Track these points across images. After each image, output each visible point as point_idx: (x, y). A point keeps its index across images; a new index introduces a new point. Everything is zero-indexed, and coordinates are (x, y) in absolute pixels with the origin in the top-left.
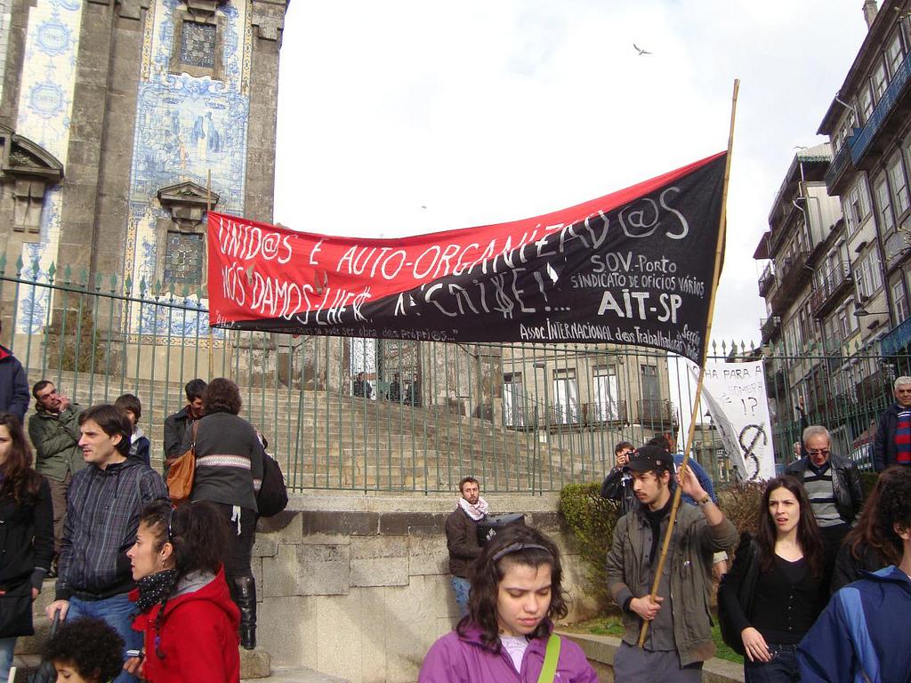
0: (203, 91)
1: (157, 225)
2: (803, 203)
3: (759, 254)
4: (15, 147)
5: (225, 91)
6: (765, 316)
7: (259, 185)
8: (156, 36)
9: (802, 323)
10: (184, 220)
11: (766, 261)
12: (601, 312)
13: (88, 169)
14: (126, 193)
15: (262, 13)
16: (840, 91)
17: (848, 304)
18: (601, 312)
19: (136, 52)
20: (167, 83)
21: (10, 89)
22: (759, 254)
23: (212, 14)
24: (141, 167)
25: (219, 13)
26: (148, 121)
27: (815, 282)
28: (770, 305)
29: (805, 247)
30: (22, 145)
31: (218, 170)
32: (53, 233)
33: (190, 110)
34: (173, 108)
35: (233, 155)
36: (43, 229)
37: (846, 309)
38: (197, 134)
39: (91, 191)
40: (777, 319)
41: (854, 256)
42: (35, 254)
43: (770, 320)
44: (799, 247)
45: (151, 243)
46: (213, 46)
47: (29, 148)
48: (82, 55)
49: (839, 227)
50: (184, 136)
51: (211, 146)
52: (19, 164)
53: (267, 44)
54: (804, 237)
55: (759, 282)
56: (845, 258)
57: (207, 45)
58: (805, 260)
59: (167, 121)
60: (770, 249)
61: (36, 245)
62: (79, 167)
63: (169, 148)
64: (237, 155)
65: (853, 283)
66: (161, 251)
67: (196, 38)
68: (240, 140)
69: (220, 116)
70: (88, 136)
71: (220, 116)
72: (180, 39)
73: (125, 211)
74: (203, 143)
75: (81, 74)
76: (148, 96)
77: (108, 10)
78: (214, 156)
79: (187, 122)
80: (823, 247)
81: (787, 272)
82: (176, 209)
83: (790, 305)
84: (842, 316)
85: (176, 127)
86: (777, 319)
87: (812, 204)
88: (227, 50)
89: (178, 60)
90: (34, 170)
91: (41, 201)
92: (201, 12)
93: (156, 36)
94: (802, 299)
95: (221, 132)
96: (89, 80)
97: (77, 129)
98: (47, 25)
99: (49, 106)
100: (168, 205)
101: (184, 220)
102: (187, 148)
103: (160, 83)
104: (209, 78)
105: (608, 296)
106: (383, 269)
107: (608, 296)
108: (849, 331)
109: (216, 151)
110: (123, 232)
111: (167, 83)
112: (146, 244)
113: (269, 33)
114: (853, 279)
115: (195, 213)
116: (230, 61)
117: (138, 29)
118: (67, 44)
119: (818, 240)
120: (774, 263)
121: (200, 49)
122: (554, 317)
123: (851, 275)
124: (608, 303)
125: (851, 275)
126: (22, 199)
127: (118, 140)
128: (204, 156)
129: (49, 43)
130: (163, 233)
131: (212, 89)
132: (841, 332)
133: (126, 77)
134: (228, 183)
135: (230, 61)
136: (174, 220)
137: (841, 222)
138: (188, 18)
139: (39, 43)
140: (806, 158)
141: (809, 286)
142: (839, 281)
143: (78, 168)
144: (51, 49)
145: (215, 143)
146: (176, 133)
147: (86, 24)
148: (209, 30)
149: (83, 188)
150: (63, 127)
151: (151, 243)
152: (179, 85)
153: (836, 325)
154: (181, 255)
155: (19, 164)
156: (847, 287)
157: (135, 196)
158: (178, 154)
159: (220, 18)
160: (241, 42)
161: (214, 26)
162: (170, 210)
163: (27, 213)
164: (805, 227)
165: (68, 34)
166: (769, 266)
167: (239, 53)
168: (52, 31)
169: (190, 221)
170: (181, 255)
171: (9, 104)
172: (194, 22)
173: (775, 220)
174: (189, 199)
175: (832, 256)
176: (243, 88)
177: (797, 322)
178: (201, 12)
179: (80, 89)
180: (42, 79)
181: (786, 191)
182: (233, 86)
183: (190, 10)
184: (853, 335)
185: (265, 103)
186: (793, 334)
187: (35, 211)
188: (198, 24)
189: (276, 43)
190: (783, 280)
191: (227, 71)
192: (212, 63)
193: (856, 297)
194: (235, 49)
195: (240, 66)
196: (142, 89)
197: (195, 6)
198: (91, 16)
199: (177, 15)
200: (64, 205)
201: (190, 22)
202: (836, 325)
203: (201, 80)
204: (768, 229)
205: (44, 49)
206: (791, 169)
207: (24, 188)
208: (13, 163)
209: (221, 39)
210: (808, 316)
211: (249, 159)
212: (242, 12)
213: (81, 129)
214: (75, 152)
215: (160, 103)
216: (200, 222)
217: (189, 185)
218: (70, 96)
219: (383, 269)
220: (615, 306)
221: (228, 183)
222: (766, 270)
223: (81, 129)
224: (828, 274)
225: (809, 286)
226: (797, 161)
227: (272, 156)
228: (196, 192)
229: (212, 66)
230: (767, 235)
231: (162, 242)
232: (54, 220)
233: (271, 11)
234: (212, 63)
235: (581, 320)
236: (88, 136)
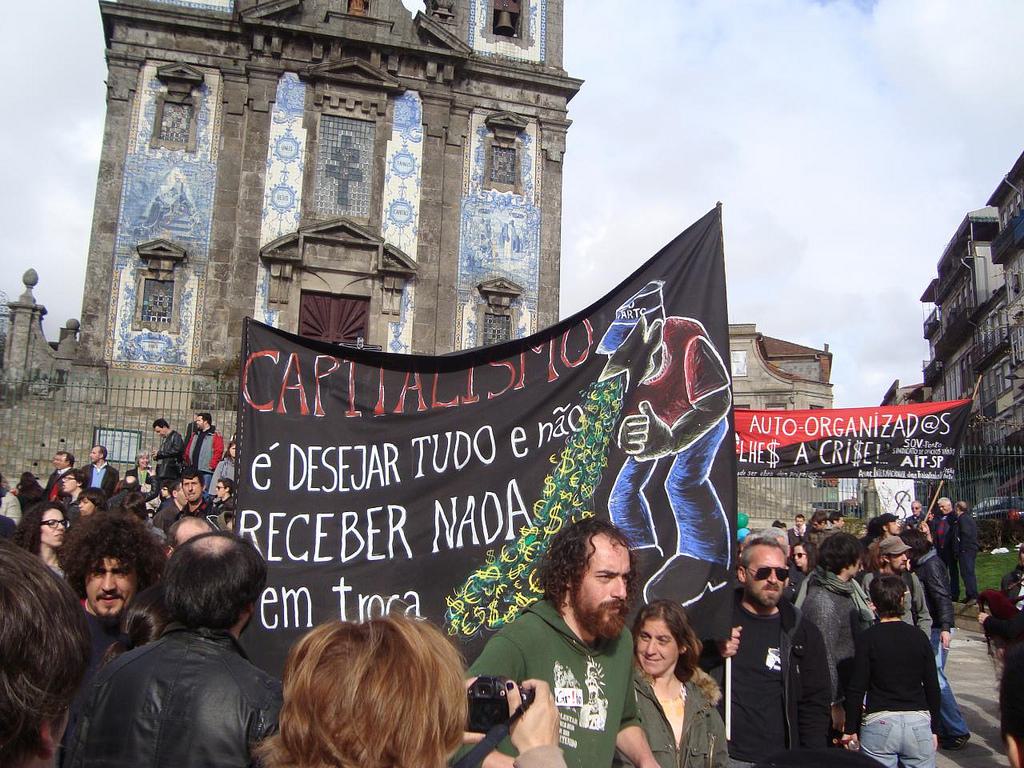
0: (507, 203)
1: (476, 309)
2: (971, 262)
3: (926, 298)
4: (386, 251)
5: (523, 203)
6: (928, 358)
7: (549, 278)
8: (472, 159)
9: (963, 372)
10: (497, 306)
11: (932, 306)
12: (902, 465)
13: (432, 267)
14: (455, 284)
15: (549, 139)
16: (1009, 174)
17: (1004, 363)
18: (902, 465)
19: (459, 171)
20: (481, 197)
21: (376, 206)
22: (926, 298)
23: (513, 141)
24: (465, 264)
25: (518, 139)
26: (468, 227)
27: (976, 336)
28: (933, 349)
29: (970, 302)
30: (390, 251)
31: (516, 265)
32: (409, 315)
33: (499, 218)
34: (486, 217)
35: (530, 254)
36: (402, 312)
37: (1002, 367)
38: (504, 238)
39: (434, 284)
40: (939, 364)
41: (1012, 322)
42: (397, 331)
43: (933, 363)
44: (964, 300)
45: (474, 323)
46: (513, 167)
47: (395, 253)
48: (424, 178)
49: (1001, 293)
50: (495, 240)
51: (514, 248)
52: (389, 266)
53: (552, 165)
54: (969, 292)
55: (925, 325)
56: (1005, 322)
57: (509, 166)
58: (968, 316)
59: (482, 227)
60: (937, 295)
61: (397, 325)
62: (426, 265)
63: (484, 249)
64: (533, 255)
65: (1009, 345)
66: (481, 328)
67: (500, 160)
68: (534, 243)
69: (520, 223)
70: (431, 241)
71: (520, 223)
72: (490, 160)
73: (454, 298)
74: (508, 245)
75: (424, 193)
76: (469, 208)
77: (441, 142)
78: (516, 256)
79: (497, 229)
80: (986, 307)
81: (952, 321)
82: (491, 297)
83: (953, 353)
84: (999, 372)
85: (489, 232)
86: (939, 364)
87: (979, 263)
88: (524, 170)
89: (489, 179)
90: (399, 270)
91: (400, 292)
92: (505, 140)
93: (472, 159)
94: (964, 350)
95: (521, 236)
96: (430, 197)
97: (422, 236)
98: (399, 155)
99: (403, 218)
100: (485, 294)
101: (497, 306)
102: (496, 249)
103: (476, 197)
104: (511, 193)
105: (908, 458)
106: (784, 429)
107: (908, 458)
108: (1004, 387)
109: (518, 251)
110: (453, 314)
111: (481, 197)
112: (469, 323)
113: (554, 156)
114: (1010, 341)
115: (505, 301)
116: (526, 178)
117: (459, 154)
118: (413, 169)
119: (982, 299)
120: (940, 309)
121: (504, 169)
122: (879, 467)
123: (1008, 338)
124: (907, 460)
125: (1008, 338)
126: (388, 290)
127: (448, 242)
128: (509, 256)
129: (402, 169)
130: (481, 315)
131: (513, 202)
132: (997, 389)
133: (452, 192)
134: (526, 276)
135: (526, 178)
136: (489, 305)
137: (1003, 289)
138: (494, 144)
139: (394, 169)
140: (976, 218)
141: (971, 339)
142: (997, 342)
143: (425, 266)
144: (404, 174)
145: (517, 245)
146: (489, 237)
147: (426, 153)
148: (511, 153)
149: (429, 281)
150: (412, 234)
151: (474, 323)
152: (490, 199)
153: (992, 378)
154: (494, 331)
155: (389, 266)
156: (1004, 348)
157: (461, 287)
158: (491, 254)
159: (518, 144)
160: (533, 163)
161: (514, 150)
162: (487, 298)
163: (391, 300)
164: (971, 284)
165: (414, 161)
166: (935, 311)
167: (533, 172)
168: (402, 159)
169: (501, 306)
170: (494, 331)
171: (376, 217)
172: (500, 147)
173: (945, 267)
174: (502, 290)
175: (993, 317)
176: (536, 201)
177: (958, 369)
178: (505, 140)
179: (424, 204)
180: (397, 197)
181: (957, 243)
182: (529, 199)
183: (496, 138)
184: (1006, 391)
185: (553, 213)
186: (954, 380)
187: (397, 299)
188: (501, 149)
189: (559, 163)
190: (947, 330)
191: (524, 187)
192: (513, 179)
193: (1011, 359)
194: (530, 169)
195: (533, 183)
196: (464, 202)
197: (501, 135)
198: (430, 146)
199: (487, 141)
200: (416, 294)
201: (496, 147)
202: (992, 378)
203: (506, 194)
204: (936, 275)
205: (398, 173)
206: (961, 227)
207: (390, 282)
208: (385, 265)
209: (519, 160)
210: (968, 366)
211: (541, 258)
212: (534, 138)
213: (426, 236)
214: (421, 250)
215: (477, 214)
216: (508, 307)
217: (502, 279)
218: (417, 210)
219: (784, 429)
220: (910, 462)
221: (526, 276)
222: (933, 314)
223: (426, 236)
224: (988, 331)
225: (971, 339)
226: (968, 220)
227: (558, 255)
228: (506, 285)
229: (513, 183)
230: (935, 282)
231: (481, 322)
232: (409, 305)
233: (556, 138)
234: (513, 179)
235: (891, 469)
236: (431, 241)
